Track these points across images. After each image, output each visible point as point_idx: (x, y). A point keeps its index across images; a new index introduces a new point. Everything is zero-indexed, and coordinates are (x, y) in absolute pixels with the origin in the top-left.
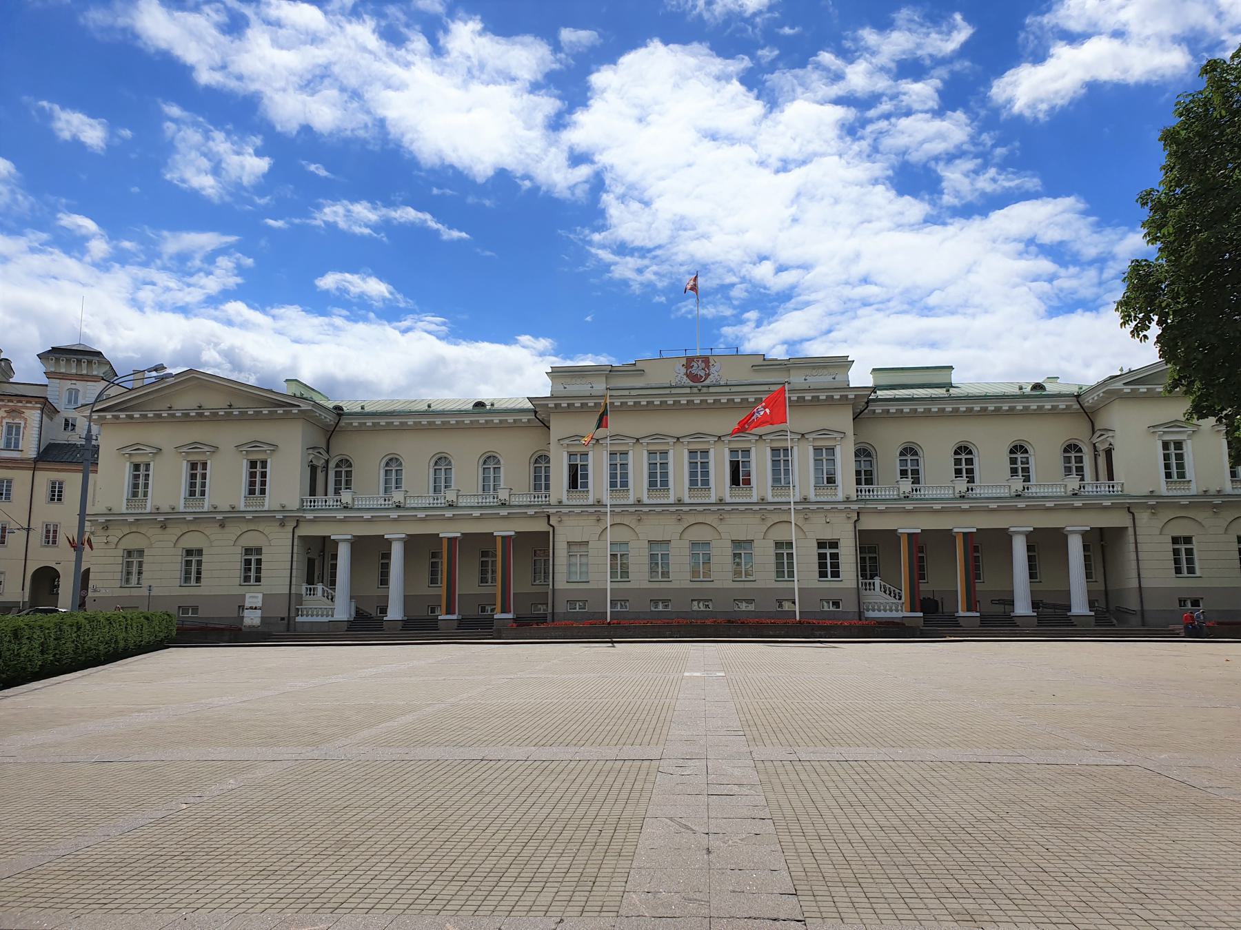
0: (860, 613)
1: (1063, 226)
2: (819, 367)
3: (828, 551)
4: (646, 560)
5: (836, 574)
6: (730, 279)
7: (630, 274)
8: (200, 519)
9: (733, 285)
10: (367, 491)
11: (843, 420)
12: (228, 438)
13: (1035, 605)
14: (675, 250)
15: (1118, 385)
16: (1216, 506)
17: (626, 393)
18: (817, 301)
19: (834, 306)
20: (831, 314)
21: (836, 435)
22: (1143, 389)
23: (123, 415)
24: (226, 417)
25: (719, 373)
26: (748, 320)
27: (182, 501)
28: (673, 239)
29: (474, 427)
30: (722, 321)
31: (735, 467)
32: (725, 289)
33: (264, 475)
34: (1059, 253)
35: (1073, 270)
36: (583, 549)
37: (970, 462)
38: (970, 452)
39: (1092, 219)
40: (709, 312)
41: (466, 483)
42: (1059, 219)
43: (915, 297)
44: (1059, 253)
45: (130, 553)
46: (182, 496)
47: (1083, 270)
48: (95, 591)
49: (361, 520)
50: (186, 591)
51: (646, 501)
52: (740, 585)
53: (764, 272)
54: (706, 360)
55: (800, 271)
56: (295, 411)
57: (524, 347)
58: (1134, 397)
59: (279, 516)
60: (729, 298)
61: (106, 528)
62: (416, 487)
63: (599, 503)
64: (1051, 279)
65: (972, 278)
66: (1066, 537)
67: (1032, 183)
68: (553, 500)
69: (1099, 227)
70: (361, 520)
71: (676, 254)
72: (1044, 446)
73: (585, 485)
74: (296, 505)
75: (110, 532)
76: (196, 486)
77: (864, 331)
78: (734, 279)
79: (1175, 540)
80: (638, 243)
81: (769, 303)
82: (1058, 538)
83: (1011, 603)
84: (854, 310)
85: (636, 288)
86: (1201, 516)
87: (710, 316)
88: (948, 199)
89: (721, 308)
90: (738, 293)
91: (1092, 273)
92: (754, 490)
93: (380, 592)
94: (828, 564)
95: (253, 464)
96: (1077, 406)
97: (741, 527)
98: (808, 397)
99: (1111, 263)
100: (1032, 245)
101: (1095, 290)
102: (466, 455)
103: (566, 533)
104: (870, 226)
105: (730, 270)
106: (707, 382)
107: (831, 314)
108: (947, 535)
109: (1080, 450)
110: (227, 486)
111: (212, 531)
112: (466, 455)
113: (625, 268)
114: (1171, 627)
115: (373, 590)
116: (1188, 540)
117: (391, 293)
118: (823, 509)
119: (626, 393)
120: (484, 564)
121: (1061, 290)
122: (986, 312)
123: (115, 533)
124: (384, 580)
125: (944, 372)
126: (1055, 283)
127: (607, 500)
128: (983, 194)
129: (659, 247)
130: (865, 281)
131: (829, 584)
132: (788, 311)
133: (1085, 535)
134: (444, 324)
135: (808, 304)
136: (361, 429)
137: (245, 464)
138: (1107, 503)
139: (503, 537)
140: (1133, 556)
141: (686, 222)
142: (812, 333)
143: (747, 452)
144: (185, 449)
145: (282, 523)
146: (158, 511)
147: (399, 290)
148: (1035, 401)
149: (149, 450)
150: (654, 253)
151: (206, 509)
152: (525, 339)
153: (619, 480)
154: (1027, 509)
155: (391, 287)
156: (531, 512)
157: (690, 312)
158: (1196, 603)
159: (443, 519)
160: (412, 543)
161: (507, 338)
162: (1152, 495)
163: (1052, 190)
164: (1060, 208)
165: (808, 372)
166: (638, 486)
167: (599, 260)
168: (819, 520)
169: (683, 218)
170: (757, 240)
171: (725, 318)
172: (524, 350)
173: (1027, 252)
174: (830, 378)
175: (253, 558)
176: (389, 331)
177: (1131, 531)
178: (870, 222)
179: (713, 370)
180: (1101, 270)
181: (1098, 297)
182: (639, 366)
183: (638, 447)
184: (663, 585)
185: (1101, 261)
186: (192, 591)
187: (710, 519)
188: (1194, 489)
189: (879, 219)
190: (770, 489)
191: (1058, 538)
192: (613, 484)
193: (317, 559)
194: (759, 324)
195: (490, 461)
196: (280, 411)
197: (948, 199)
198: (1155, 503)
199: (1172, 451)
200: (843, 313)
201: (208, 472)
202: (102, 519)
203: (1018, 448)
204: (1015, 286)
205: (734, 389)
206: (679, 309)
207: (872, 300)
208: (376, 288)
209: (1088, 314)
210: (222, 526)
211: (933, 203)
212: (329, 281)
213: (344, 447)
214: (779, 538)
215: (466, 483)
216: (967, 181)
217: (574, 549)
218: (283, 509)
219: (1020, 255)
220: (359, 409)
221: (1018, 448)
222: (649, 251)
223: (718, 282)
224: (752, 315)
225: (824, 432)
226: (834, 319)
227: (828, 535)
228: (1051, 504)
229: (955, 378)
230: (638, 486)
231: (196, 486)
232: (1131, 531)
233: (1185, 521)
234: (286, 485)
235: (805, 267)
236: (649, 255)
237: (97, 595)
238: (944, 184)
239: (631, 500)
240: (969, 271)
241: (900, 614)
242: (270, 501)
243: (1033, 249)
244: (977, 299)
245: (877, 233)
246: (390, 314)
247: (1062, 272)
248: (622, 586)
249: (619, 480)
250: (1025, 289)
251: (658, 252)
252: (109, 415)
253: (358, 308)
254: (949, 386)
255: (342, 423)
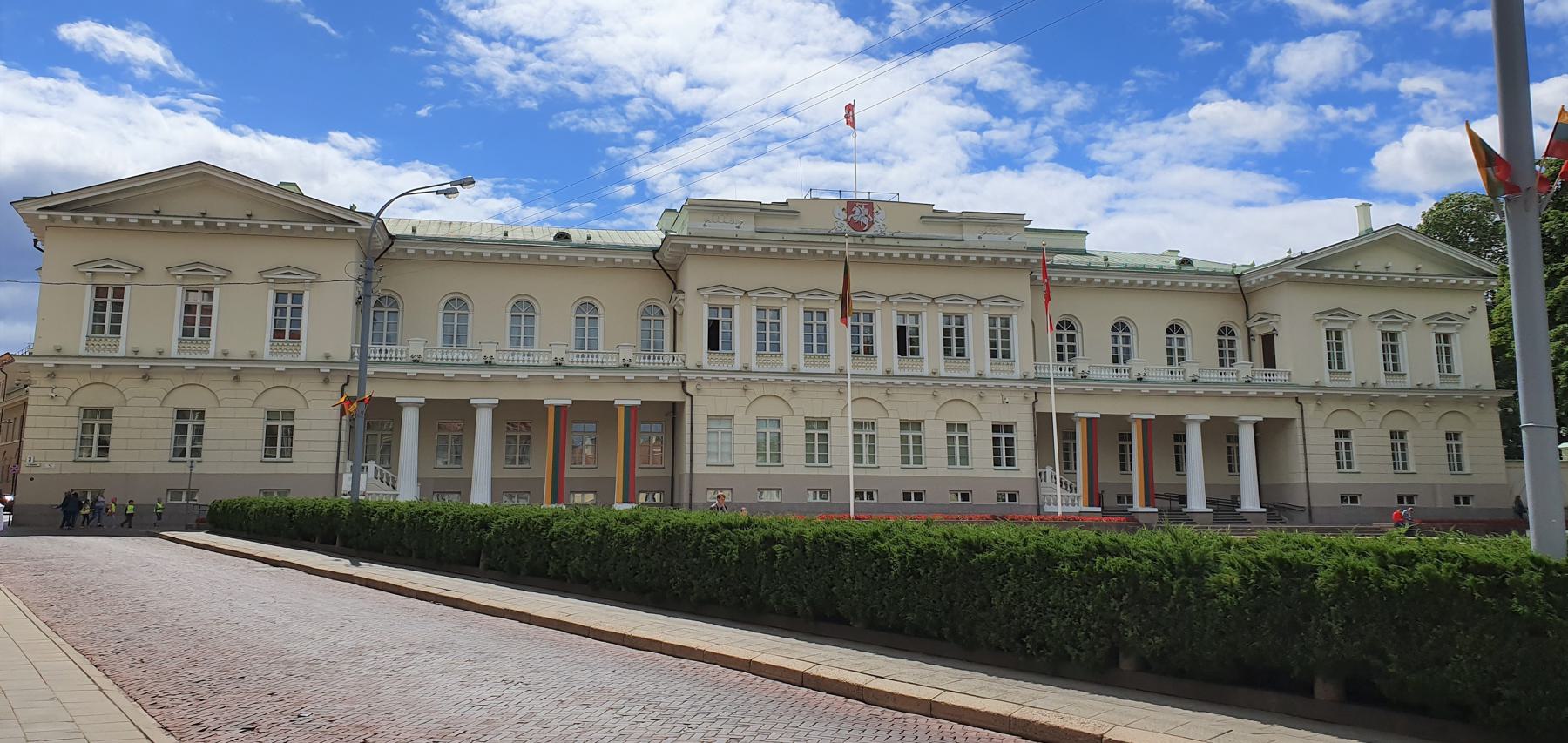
0: (1039, 508)
1: (1005, 75)
2: (994, 225)
3: (1003, 436)
4: (262, 435)
5: (1010, 463)
6: (631, 90)
7: (498, 69)
8: (202, 369)
9: (631, 97)
10: (422, 338)
11: (1018, 286)
12: (248, 259)
13: (1209, 502)
14: (569, 46)
15: (1291, 268)
16: (1373, 399)
17: (937, 244)
18: (727, 129)
19: (743, 135)
20: (740, 145)
21: (1013, 303)
22: (1313, 274)
23: (88, 217)
24: (252, 232)
25: (882, 223)
26: (641, 142)
27: (175, 343)
28: (571, 31)
29: (554, 265)
30: (609, 139)
31: (713, 326)
32: (620, 101)
33: (118, 307)
34: (998, 104)
35: (1006, 121)
36: (726, 424)
37: (1071, 338)
38: (1072, 328)
39: (1034, 70)
40: (596, 125)
41: (555, 337)
42: (1003, 66)
43: (834, 136)
44: (998, 104)
45: (182, 414)
46: (84, 334)
47: (1016, 122)
48: (32, 465)
49: (443, 379)
50: (82, 468)
51: (802, 369)
52: (765, 471)
53: (671, 87)
54: (869, 205)
55: (712, 90)
56: (351, 229)
57: (334, 146)
58: (1303, 281)
59: (325, 369)
60: (623, 114)
61: (52, 375)
62: (489, 334)
63: (841, 373)
64: (982, 128)
65: (899, 121)
66: (1237, 427)
67: (983, 22)
68: (690, 364)
69: (1040, 80)
70: (443, 379)
71: (572, 51)
72: (1203, 322)
73: (729, 346)
74: (347, 358)
75: (58, 382)
76: (196, 321)
77: (770, 169)
78: (633, 90)
79: (950, 426)
80: (527, 30)
81: (676, 126)
82: (464, 412)
83: (1183, 500)
84: (766, 144)
85: (503, 89)
86: (1415, 410)
87: (597, 131)
88: (894, 31)
89: (612, 122)
90: (636, 108)
91: (1025, 128)
92: (879, 360)
93: (1177, 480)
94: (1004, 453)
95: (100, 291)
96: (1236, 286)
97: (912, 405)
98: (1004, 259)
99: (1046, 118)
100: (970, 91)
101: (1025, 145)
102: (555, 303)
103: (705, 404)
104: (803, 48)
105: (631, 78)
106: (871, 231)
107: (740, 145)
108: (1123, 420)
109: (1233, 334)
110: (241, 324)
111: (222, 386)
112: (555, 303)
113: (494, 62)
114: (1375, 525)
115: (1223, 477)
116: (963, 427)
117: (165, 58)
118: (999, 386)
119: (937, 244)
120: (1122, 448)
121: (991, 142)
122: (905, 159)
123: (66, 384)
124: (1180, 464)
125: (1076, 237)
126: (985, 133)
127: (1052, 373)
128: (931, 29)
129: (553, 40)
130: (785, 111)
131: (1004, 473)
132: (692, 136)
133: (1205, 426)
134: (216, 104)
135: (716, 130)
136: (410, 259)
137: (89, 292)
138: (1279, 392)
139: (626, 407)
140: (1301, 450)
141: (589, 15)
142: (713, 165)
143: (729, 310)
144: (90, 268)
145: (326, 379)
146: (136, 355)
147: (178, 57)
148: (1183, 277)
149: (126, 269)
150: (546, 46)
151: (211, 356)
152: (339, 137)
153: (769, 341)
154: (1260, 396)
155: (170, 55)
156: (664, 376)
157: (576, 123)
158: (1354, 499)
159: (552, 381)
160: (502, 410)
161: (314, 132)
162: (1317, 386)
163: (1001, 36)
164: (1006, 55)
165: (983, 229)
166: (793, 351)
167: (462, 48)
168: (994, 399)
169: (586, 10)
170: (669, 45)
171: (614, 135)
172: (334, 151)
173: (962, 98)
174: (1005, 238)
175: (190, 424)
176: (147, 110)
177: (1298, 423)
178: (803, 44)
179: (877, 217)
180: (1035, 125)
181: (1026, 152)
182: (792, 206)
183: (979, 309)
184: (773, 471)
185: (1036, 115)
186: (279, 468)
187: (780, 391)
188: (1353, 382)
189: (816, 42)
190: (754, 356)
191: (464, 412)
192: (762, 347)
193: (372, 424)
194: (654, 147)
195: (587, 310)
196: (330, 228)
197: (894, 31)
198: (1321, 395)
199: (768, 318)
200: (752, 146)
201: (1435, 345)
202: (50, 363)
203: (1174, 328)
204: (944, 133)
205: (787, 237)
206: (561, 119)
207: (788, 134)
208: (144, 49)
209: (1010, 173)
210: (146, 377)
211: (874, 31)
212: (79, 32)
213: (391, 280)
214: (763, 414)
215: (555, 337)
216: (917, 14)
217: (714, 425)
218: (327, 360)
219: (954, 99)
220: (410, 232)
221: (1120, 326)
222: (540, 43)
223: (615, 91)
224: (647, 135)
225: (1002, 299)
226: (740, 151)
227: (1004, 418)
228: (1119, 390)
229: (1091, 244)
230: (793, 351)
231: (286, 329)
232: (1298, 423)
233: (964, 406)
234: (329, 326)
235: (721, 86)
236: (538, 49)
237: (34, 471)
238: (893, 15)
239: (785, 368)
240: (897, 113)
241: (1077, 509)
242: (308, 349)
243: (970, 95)
244: (899, 144)
245: (810, 59)
246: (155, 85)
247: (996, 124)
248: (773, 471)
249: (769, 341)
250: (950, 138)
251: (550, 46)
252: (66, 216)
253: (106, 75)
254: (1084, 253)
255: (392, 250)
